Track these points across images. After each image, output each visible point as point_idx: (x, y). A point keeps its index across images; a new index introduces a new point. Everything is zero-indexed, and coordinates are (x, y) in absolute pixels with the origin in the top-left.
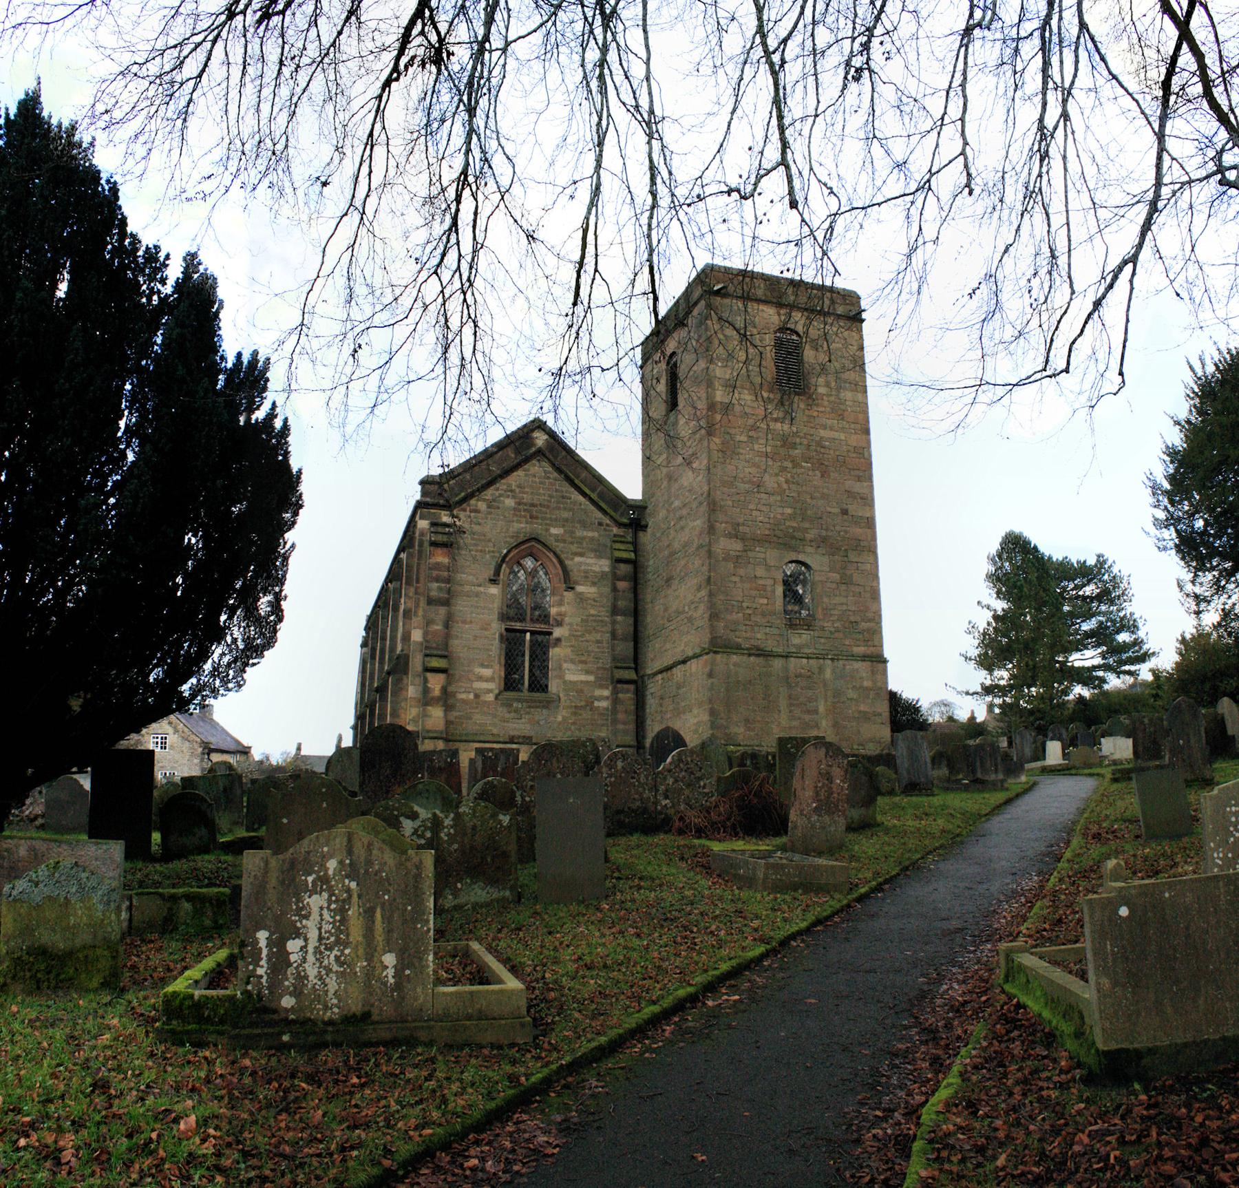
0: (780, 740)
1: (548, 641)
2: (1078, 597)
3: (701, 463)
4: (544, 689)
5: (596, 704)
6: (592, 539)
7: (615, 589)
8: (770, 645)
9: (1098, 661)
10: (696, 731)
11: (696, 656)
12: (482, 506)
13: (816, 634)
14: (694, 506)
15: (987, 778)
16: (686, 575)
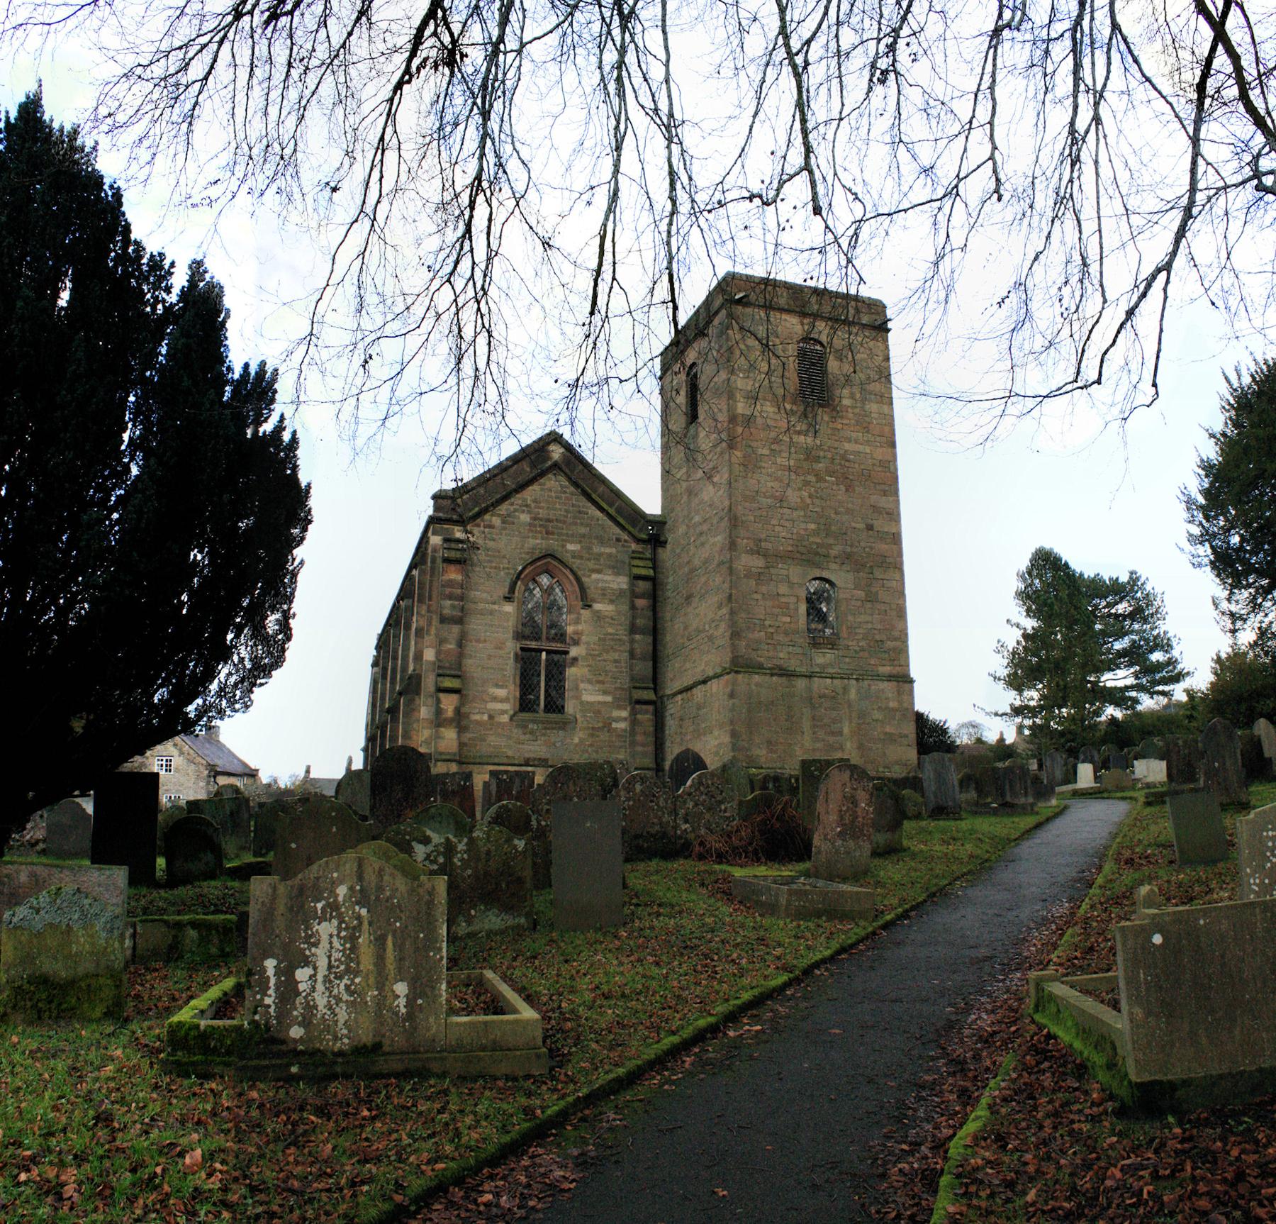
0: (804, 762)
1: (565, 661)
2: (1110, 615)
3: (721, 477)
4: (560, 709)
5: (614, 725)
6: (610, 555)
7: (633, 607)
8: (793, 665)
9: (1131, 681)
10: (717, 753)
11: (716, 676)
12: (496, 521)
13: (841, 653)
14: (715, 522)
15: (1016, 801)
16: (707, 592)
